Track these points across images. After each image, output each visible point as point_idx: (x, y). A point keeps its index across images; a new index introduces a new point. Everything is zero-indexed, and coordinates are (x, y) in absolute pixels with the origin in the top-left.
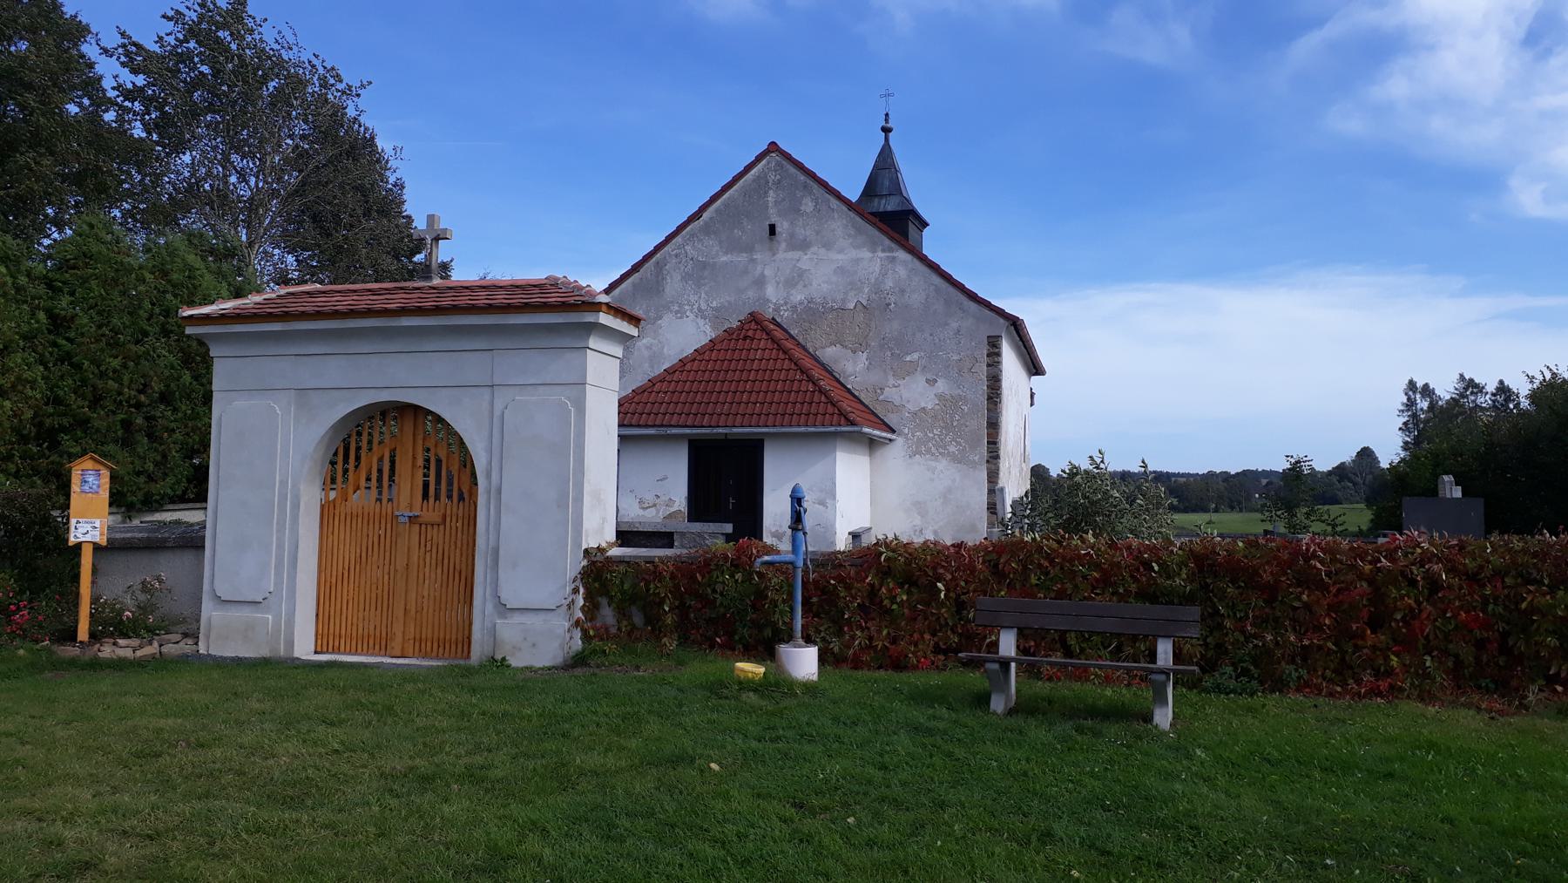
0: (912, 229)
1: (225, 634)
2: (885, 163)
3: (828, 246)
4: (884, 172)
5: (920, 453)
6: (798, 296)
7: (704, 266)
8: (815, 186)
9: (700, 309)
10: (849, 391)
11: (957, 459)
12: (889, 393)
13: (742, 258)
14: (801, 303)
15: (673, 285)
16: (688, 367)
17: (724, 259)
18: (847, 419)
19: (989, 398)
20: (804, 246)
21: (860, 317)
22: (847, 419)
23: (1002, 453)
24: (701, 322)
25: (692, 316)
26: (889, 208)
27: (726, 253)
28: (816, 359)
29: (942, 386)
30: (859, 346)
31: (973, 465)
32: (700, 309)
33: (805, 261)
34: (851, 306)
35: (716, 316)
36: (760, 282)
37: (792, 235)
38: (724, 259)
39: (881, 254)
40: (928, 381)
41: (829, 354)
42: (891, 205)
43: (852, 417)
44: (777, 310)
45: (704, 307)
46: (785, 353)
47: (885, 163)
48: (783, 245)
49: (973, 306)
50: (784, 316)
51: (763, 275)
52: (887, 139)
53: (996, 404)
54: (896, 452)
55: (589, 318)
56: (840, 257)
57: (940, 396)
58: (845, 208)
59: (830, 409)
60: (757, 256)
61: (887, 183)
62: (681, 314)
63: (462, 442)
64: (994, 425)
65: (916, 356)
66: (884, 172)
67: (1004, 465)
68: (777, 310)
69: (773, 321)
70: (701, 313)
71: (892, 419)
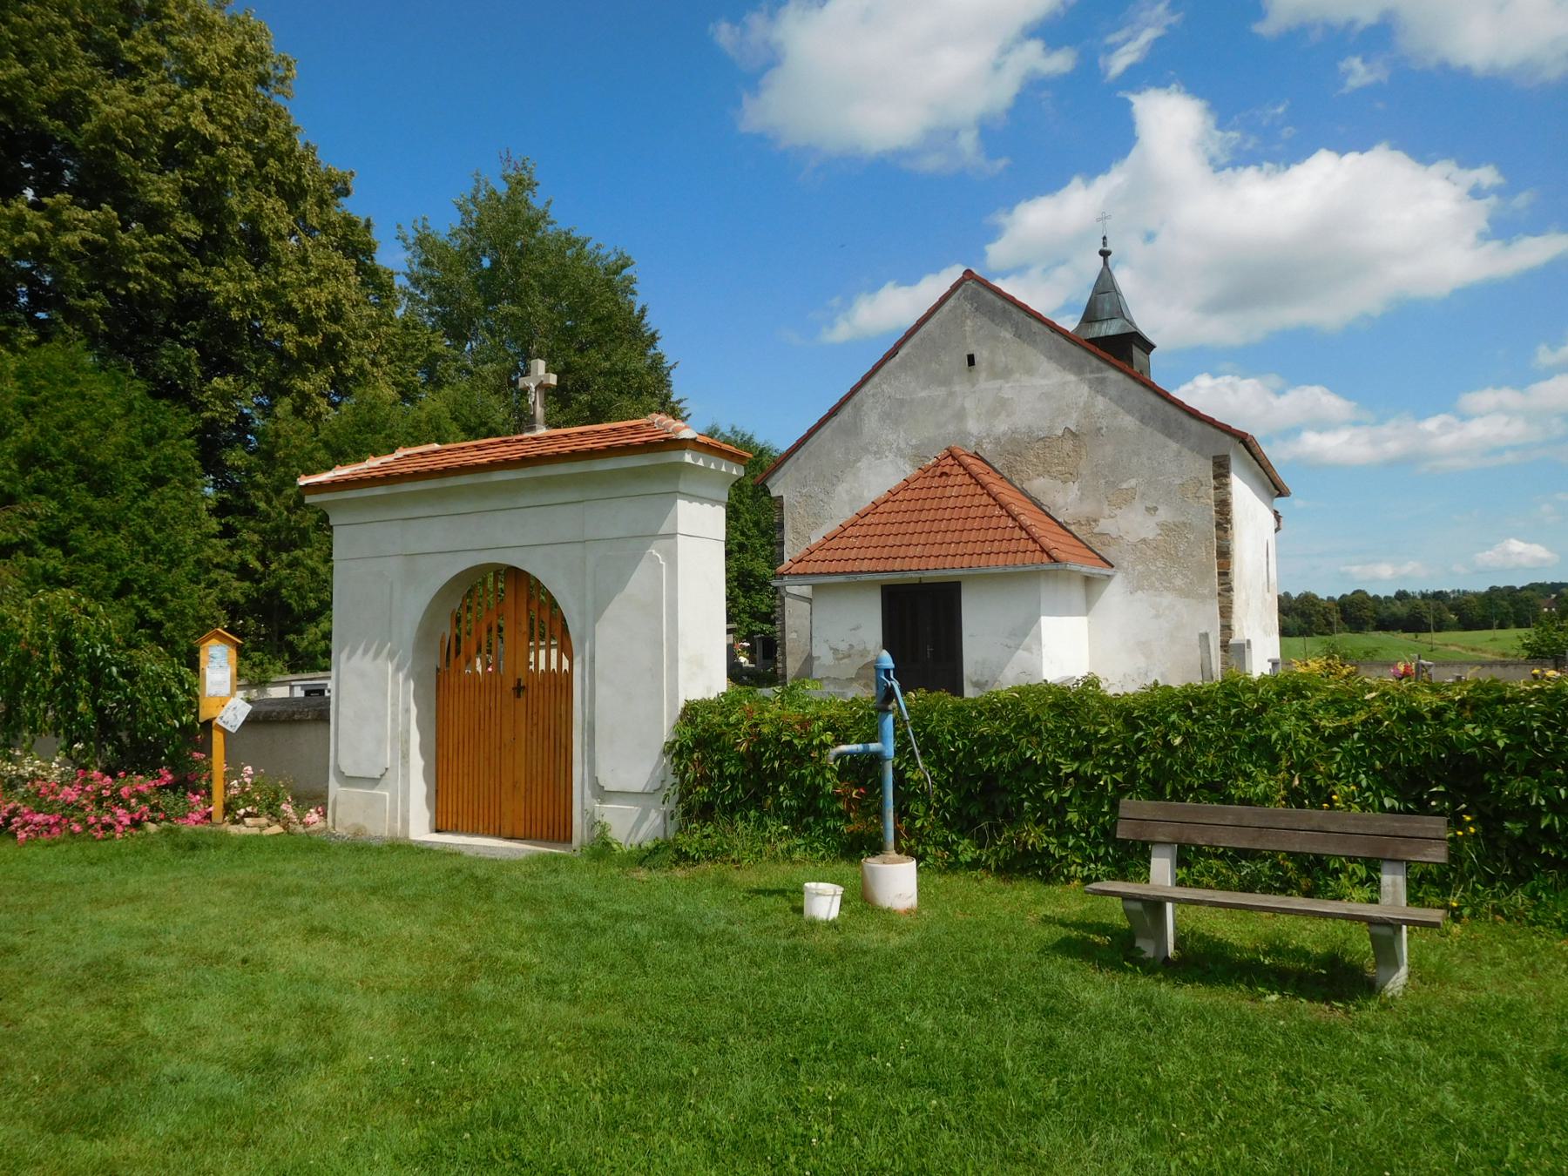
0: (1137, 353)
1: (349, 811)
2: (1105, 287)
3: (1030, 371)
4: (1104, 297)
5: (1142, 588)
6: (1002, 426)
7: (902, 403)
8: (1014, 310)
9: (898, 448)
10: (1060, 524)
11: (1184, 593)
12: (1105, 525)
13: (939, 392)
14: (1004, 434)
15: (871, 422)
16: (880, 509)
17: (923, 394)
18: (1050, 556)
19: (1219, 526)
20: (1006, 373)
21: (1068, 445)
22: (1050, 556)
23: (1235, 584)
24: (901, 462)
25: (891, 456)
26: (1111, 332)
27: (923, 389)
28: (1023, 492)
29: (1163, 514)
30: (1070, 476)
31: (1203, 598)
32: (898, 448)
33: (1008, 390)
34: (1060, 433)
35: (917, 455)
36: (960, 415)
37: (992, 365)
38: (923, 394)
39: (1089, 376)
40: (1148, 509)
41: (1038, 485)
42: (1112, 329)
43: (1055, 553)
44: (979, 444)
45: (903, 445)
46: (983, 488)
47: (1105, 287)
48: (983, 375)
49: (1194, 425)
50: (987, 449)
51: (963, 408)
52: (1105, 263)
53: (1226, 530)
54: (1114, 593)
55: (673, 457)
56: (1044, 382)
57: (1160, 525)
58: (1047, 331)
59: (1031, 546)
60: (957, 388)
61: (1107, 307)
62: (878, 454)
63: (554, 604)
64: (1224, 554)
65: (1133, 482)
66: (1104, 297)
67: (1239, 597)
68: (979, 444)
69: (977, 456)
70: (900, 453)
71: (1110, 553)
